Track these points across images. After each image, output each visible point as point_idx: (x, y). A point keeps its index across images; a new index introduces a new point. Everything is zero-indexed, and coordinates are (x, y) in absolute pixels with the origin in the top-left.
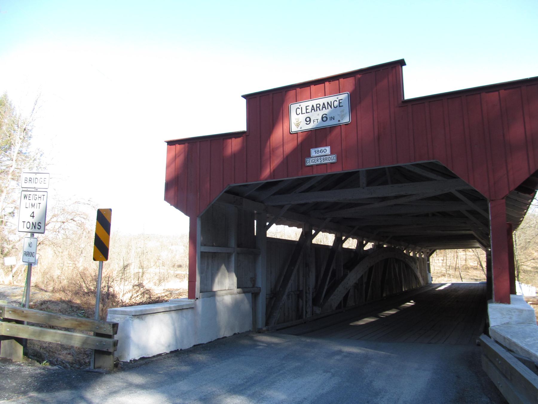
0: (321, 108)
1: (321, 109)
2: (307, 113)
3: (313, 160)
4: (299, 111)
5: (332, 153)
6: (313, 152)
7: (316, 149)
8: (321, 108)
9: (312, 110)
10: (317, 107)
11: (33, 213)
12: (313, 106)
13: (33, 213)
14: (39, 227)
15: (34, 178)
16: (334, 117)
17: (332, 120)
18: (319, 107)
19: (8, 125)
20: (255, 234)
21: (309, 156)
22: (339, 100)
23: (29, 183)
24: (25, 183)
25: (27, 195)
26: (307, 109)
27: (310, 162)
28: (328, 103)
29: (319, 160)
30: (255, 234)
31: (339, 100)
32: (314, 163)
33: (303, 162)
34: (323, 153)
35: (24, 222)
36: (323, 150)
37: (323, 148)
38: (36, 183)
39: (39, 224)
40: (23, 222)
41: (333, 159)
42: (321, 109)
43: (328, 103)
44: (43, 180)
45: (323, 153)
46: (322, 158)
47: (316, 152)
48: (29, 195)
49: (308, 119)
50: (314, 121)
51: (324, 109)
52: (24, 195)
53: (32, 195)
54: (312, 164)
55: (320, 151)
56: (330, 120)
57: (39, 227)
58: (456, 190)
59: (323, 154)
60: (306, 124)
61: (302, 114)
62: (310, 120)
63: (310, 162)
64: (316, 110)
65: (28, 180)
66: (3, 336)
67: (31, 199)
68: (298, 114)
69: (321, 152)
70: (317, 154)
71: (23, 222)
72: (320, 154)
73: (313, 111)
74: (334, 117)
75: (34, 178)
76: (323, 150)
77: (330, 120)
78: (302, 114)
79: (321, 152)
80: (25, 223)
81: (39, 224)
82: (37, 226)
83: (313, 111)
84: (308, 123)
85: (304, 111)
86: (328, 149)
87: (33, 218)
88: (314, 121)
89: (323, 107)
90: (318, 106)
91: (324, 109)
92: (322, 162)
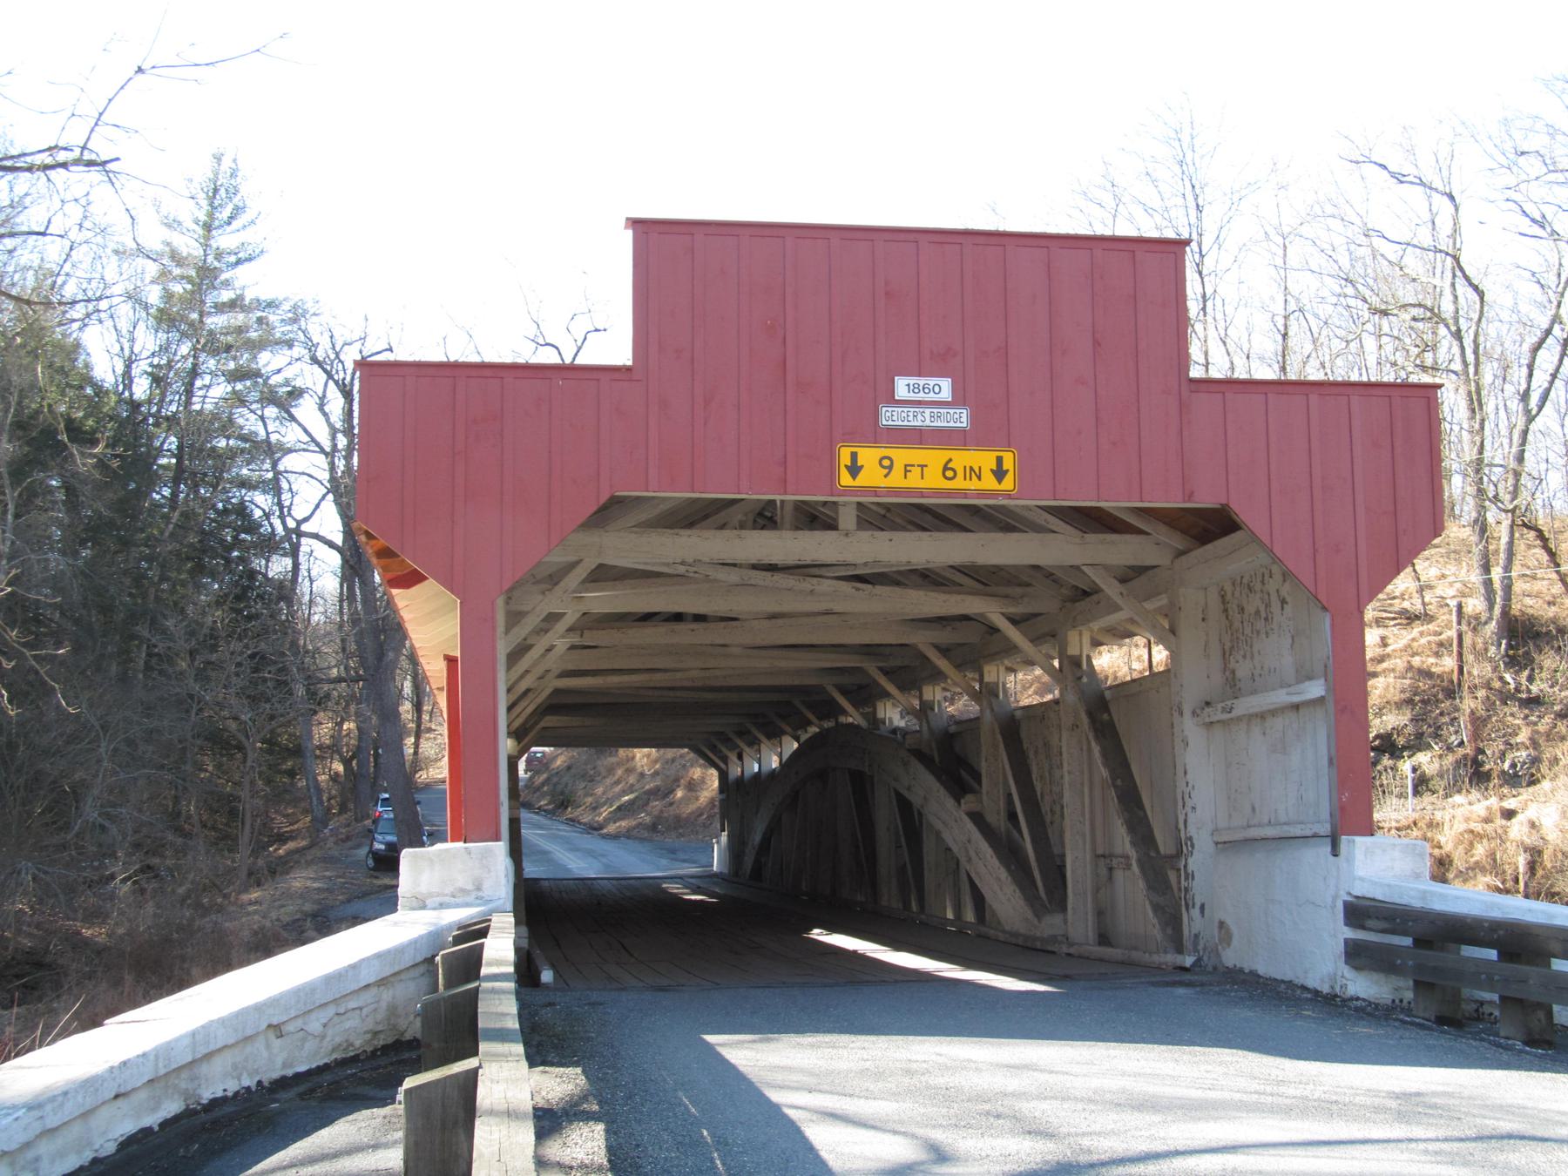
3: (903, 415)
5: (959, 400)
6: (903, 387)
7: (912, 380)
16: (980, 468)
17: (971, 479)
19: (213, 674)
20: (818, 934)
27: (973, 920)
29: (919, 417)
30: (818, 934)
32: (906, 423)
34: (932, 394)
36: (931, 387)
37: (932, 382)
45: (932, 394)
47: (912, 388)
50: (908, 468)
54: (900, 423)
55: (924, 388)
56: (965, 479)
59: (931, 397)
63: (973, 920)
69: (927, 390)
70: (912, 394)
72: (921, 396)
74: (980, 468)
76: (931, 387)
77: (965, 479)
79: (927, 390)
86: (944, 388)
88: (906, 471)
92: (928, 423)
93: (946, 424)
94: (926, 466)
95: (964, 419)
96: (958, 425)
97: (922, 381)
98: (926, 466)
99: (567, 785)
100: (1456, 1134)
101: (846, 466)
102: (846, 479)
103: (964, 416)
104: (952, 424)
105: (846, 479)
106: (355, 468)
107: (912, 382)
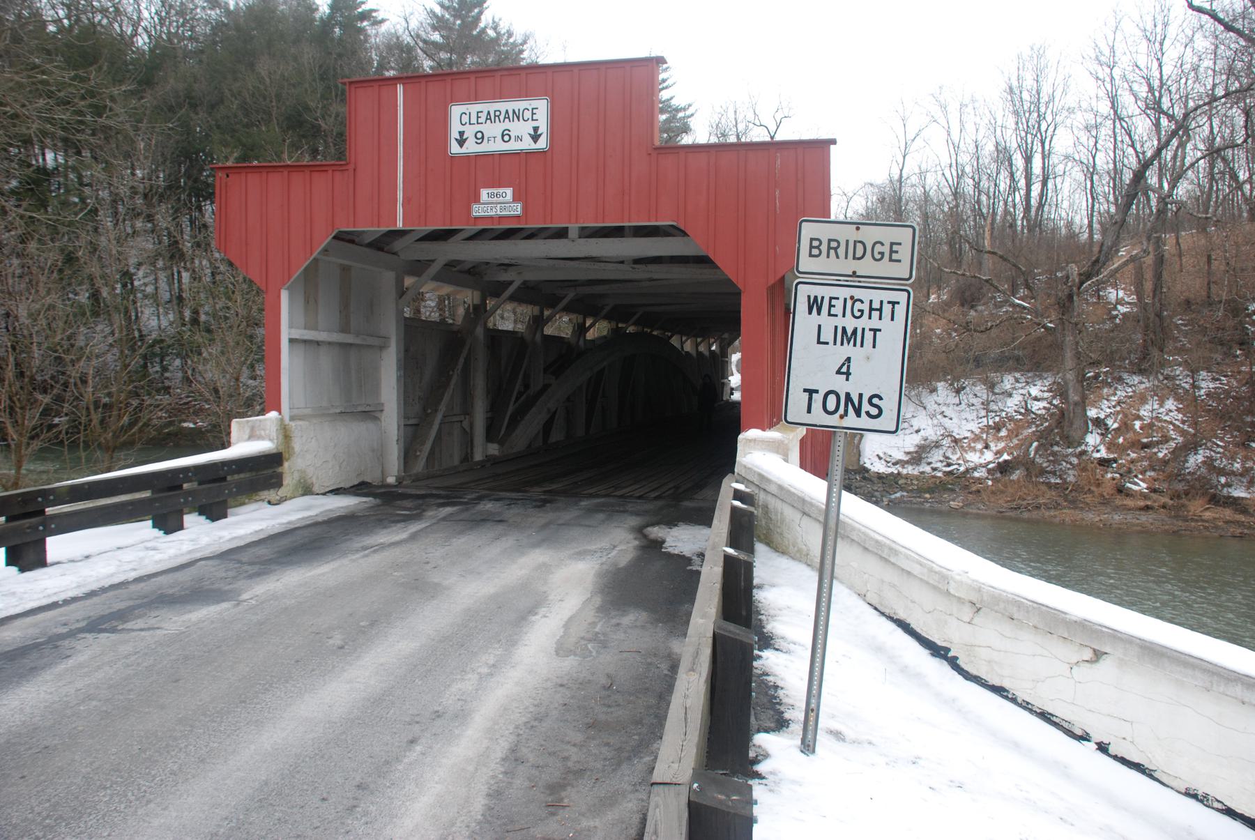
0: (502, 117)
1: (502, 120)
2: (478, 123)
4: (465, 119)
5: (515, 199)
6: (484, 193)
7: (490, 191)
8: (502, 117)
9: (487, 119)
10: (495, 116)
11: (849, 359)
12: (489, 113)
13: (849, 359)
14: (874, 411)
15: (847, 241)
18: (498, 116)
21: (477, 199)
22: (533, 109)
23: (828, 257)
24: (811, 255)
25: (823, 298)
26: (478, 117)
27: (478, 211)
28: (514, 111)
29: (494, 210)
31: (533, 109)
32: (486, 214)
33: (469, 209)
34: (501, 198)
35: (811, 392)
37: (501, 190)
38: (854, 258)
39: (875, 401)
40: (805, 390)
41: (517, 209)
42: (502, 120)
43: (514, 111)
44: (886, 249)
45: (501, 198)
46: (499, 206)
48: (831, 298)
49: (479, 135)
51: (507, 120)
52: (809, 297)
53: (841, 301)
57: (874, 411)
58: (433, 261)
60: (476, 143)
61: (470, 124)
62: (483, 138)
63: (478, 211)
64: (511, 119)
65: (824, 248)
66: (3, 619)
67: (840, 314)
68: (464, 123)
71: (805, 390)
73: (489, 121)
75: (847, 241)
78: (470, 124)
80: (818, 398)
81: (875, 401)
82: (866, 407)
83: (489, 121)
84: (479, 141)
85: (474, 120)
86: (509, 191)
87: (847, 379)
89: (505, 118)
90: (498, 113)
91: (507, 120)
92: (498, 213)
93: (509, 213)
94: (880, 330)
95: (519, 210)
96: (516, 213)
97: (495, 191)
98: (880, 330)
99: (497, 763)
100: (603, 264)
101: (456, 139)
102: (455, 149)
103: (519, 207)
104: (512, 213)
105: (455, 149)
106: (284, 296)
107: (490, 192)
